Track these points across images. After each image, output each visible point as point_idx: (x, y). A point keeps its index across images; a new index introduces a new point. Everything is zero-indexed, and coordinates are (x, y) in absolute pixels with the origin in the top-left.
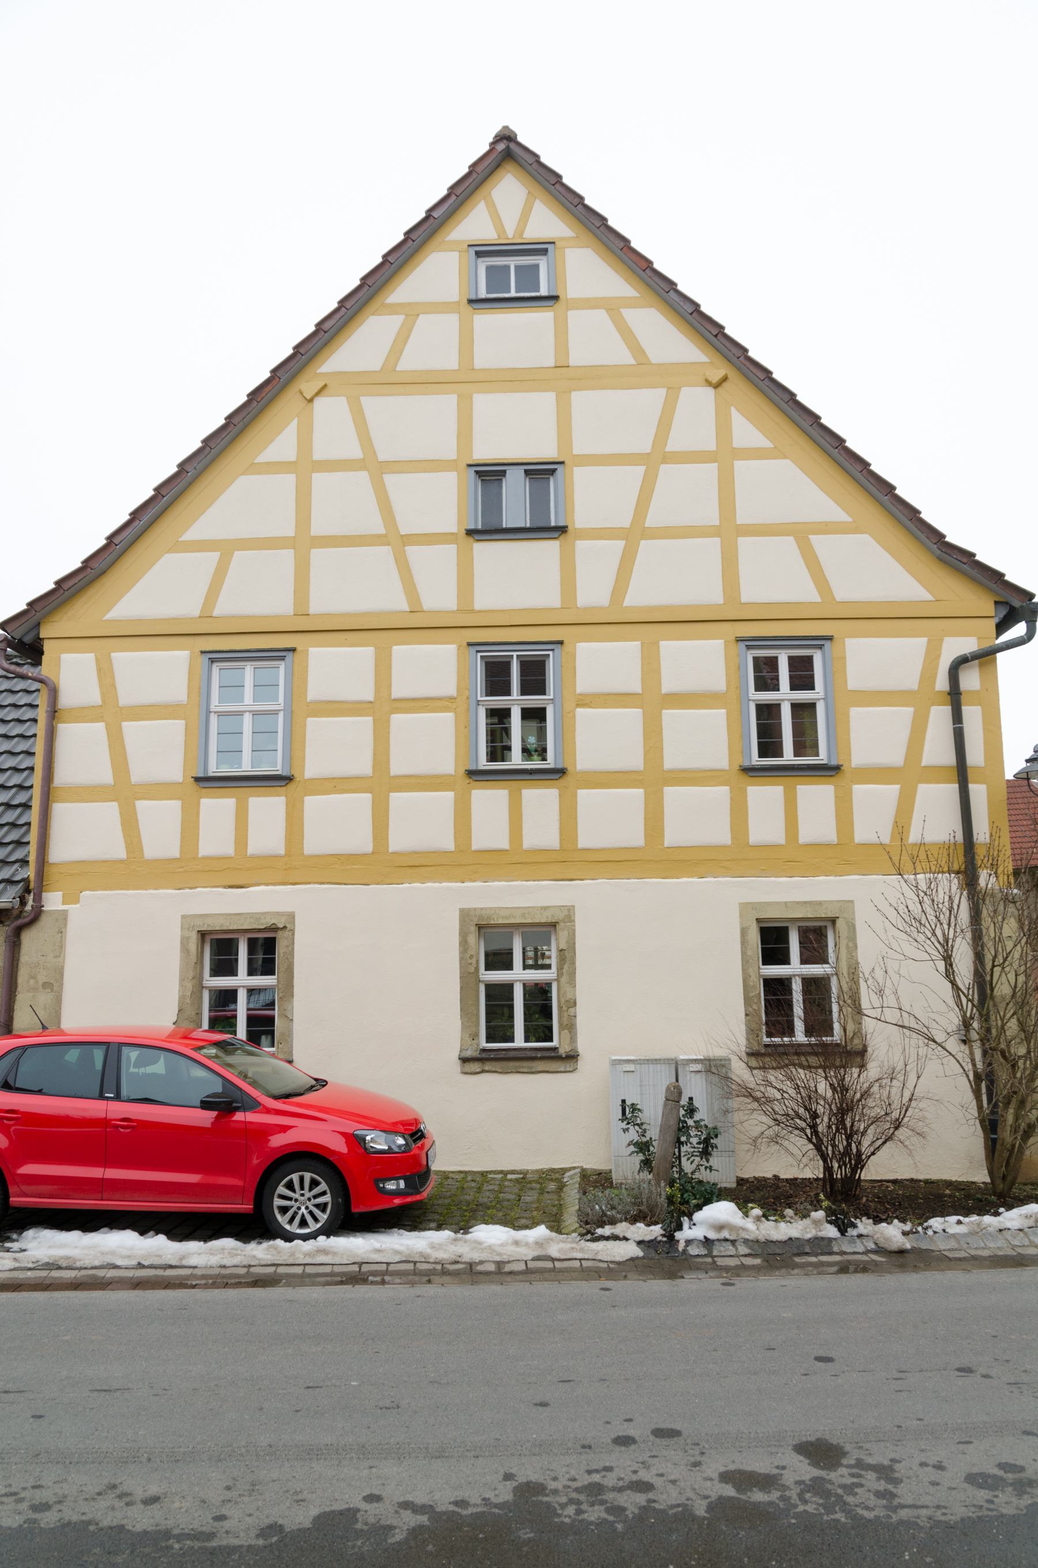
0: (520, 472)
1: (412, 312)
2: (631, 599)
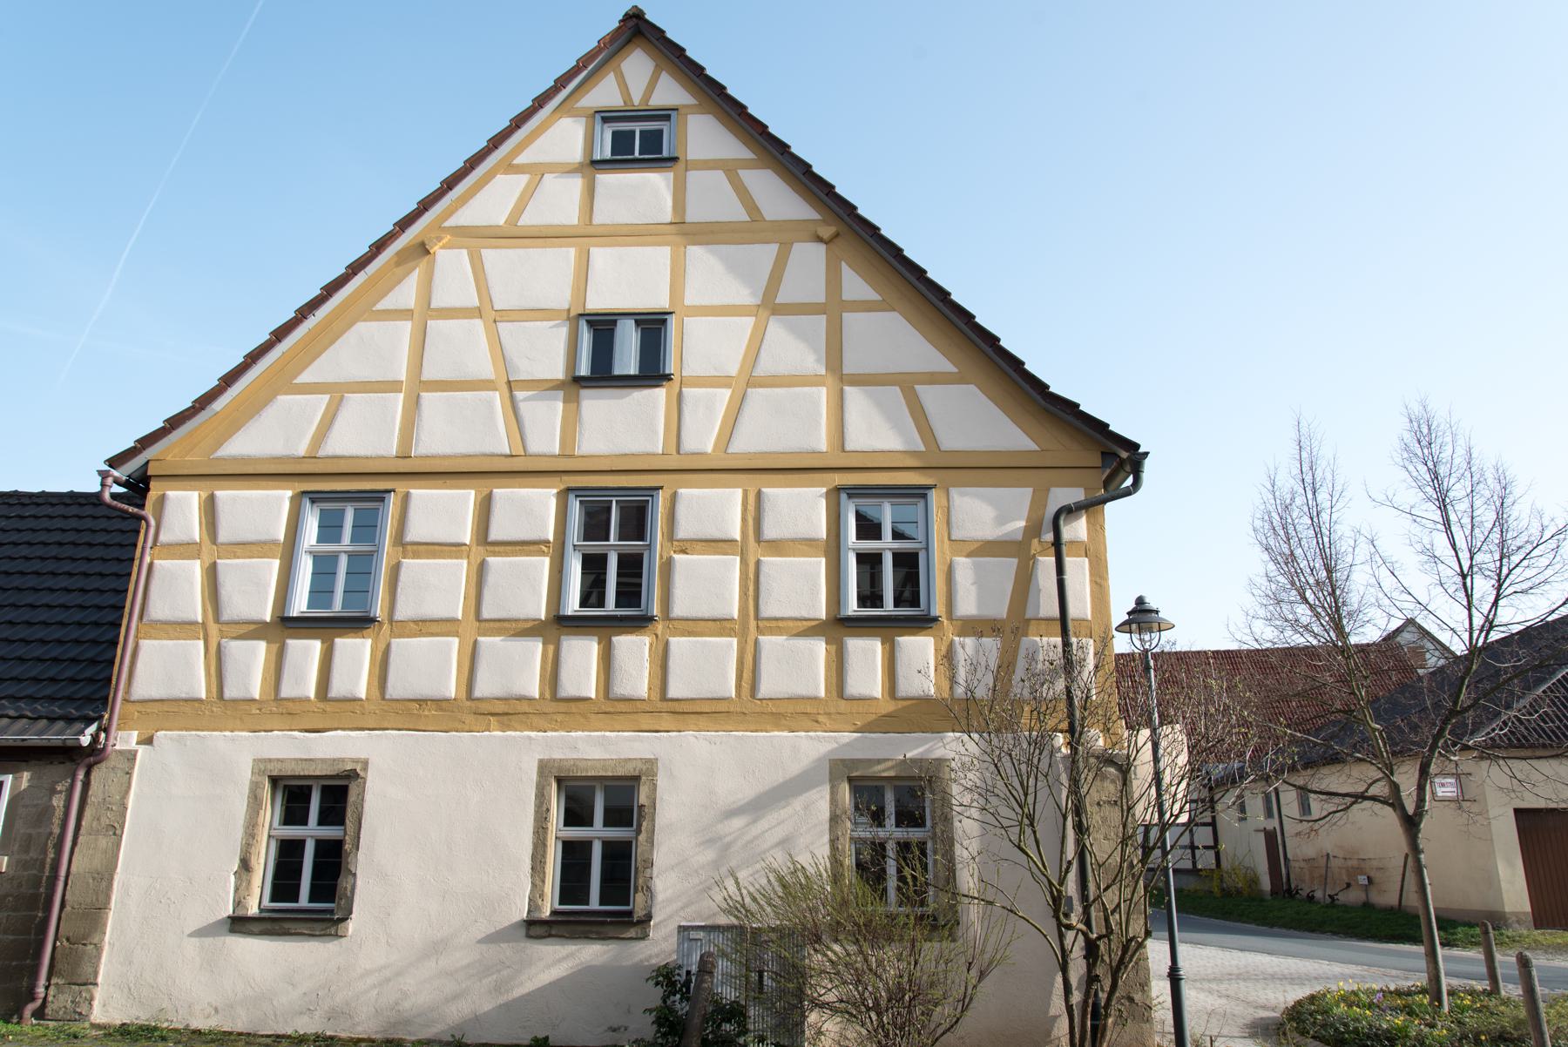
0: (631, 323)
1: (538, 171)
2: (735, 447)
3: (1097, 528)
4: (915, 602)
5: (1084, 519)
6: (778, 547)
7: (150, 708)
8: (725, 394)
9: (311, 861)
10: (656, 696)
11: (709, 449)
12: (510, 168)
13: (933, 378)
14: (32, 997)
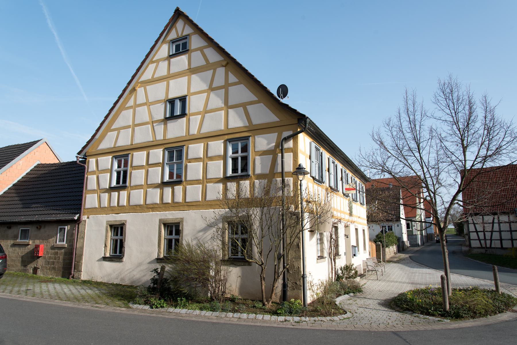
1: (158, 61)
3: (296, 143)
5: (292, 141)
6: (211, 159)
7: (89, 210)
8: (199, 117)
10: (184, 202)
11: (196, 133)
12: (152, 62)
13: (251, 103)
14: (71, 274)
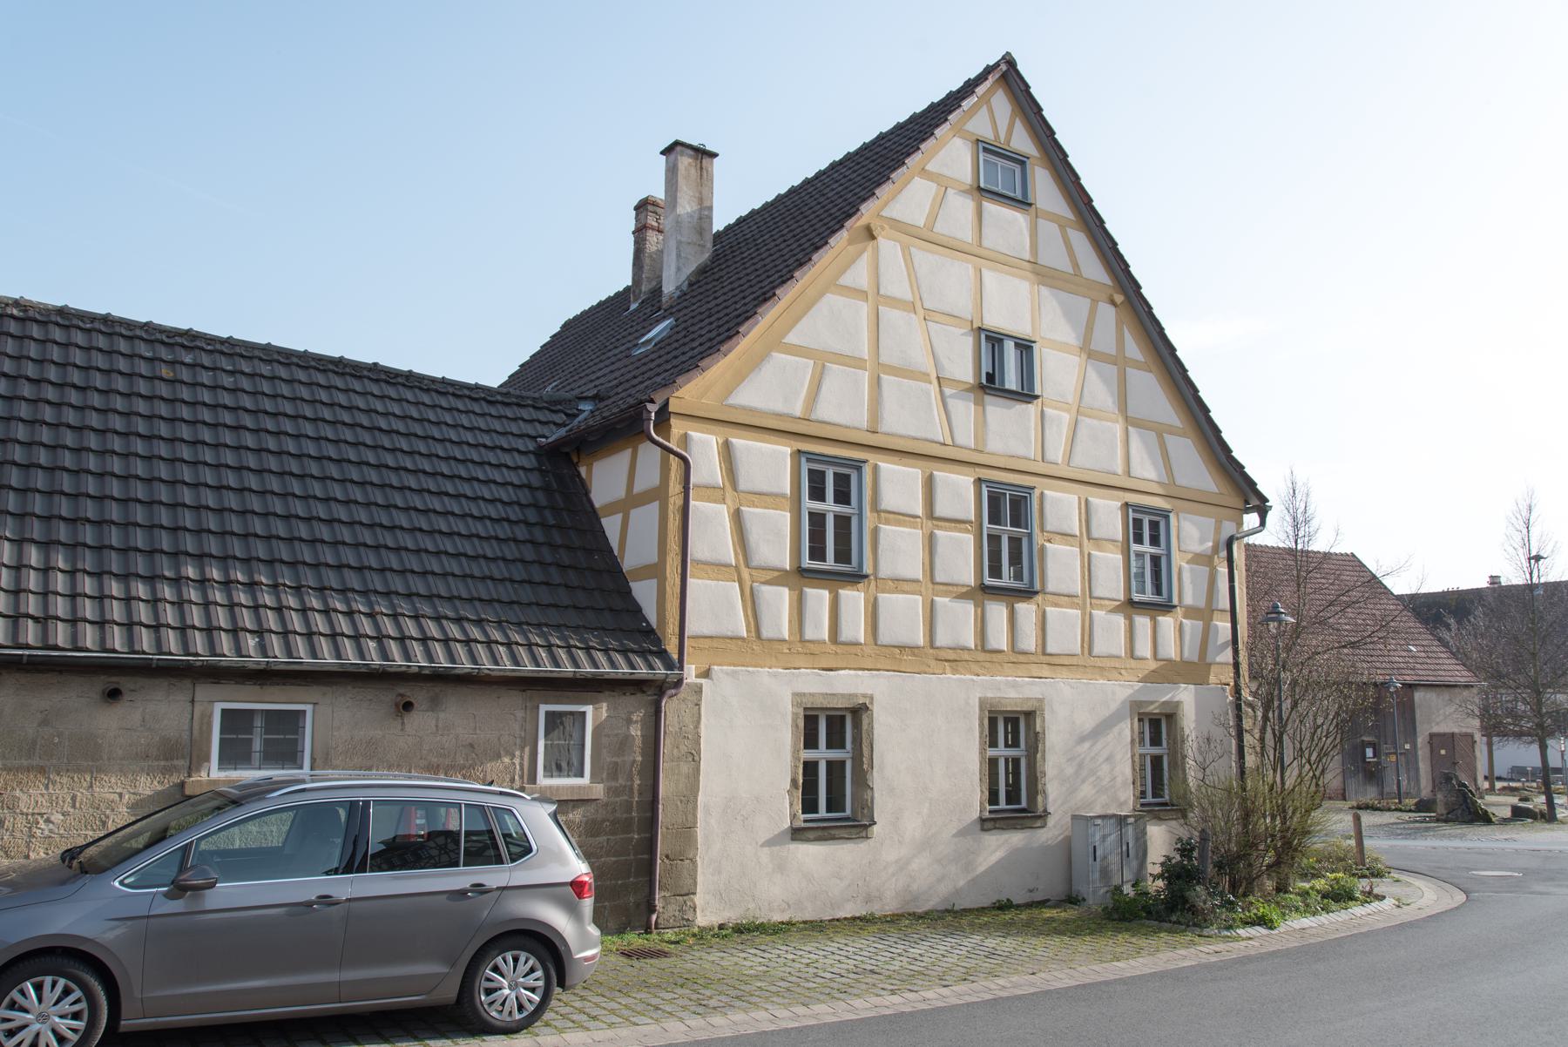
4: (848, 561)
9: (833, 779)
